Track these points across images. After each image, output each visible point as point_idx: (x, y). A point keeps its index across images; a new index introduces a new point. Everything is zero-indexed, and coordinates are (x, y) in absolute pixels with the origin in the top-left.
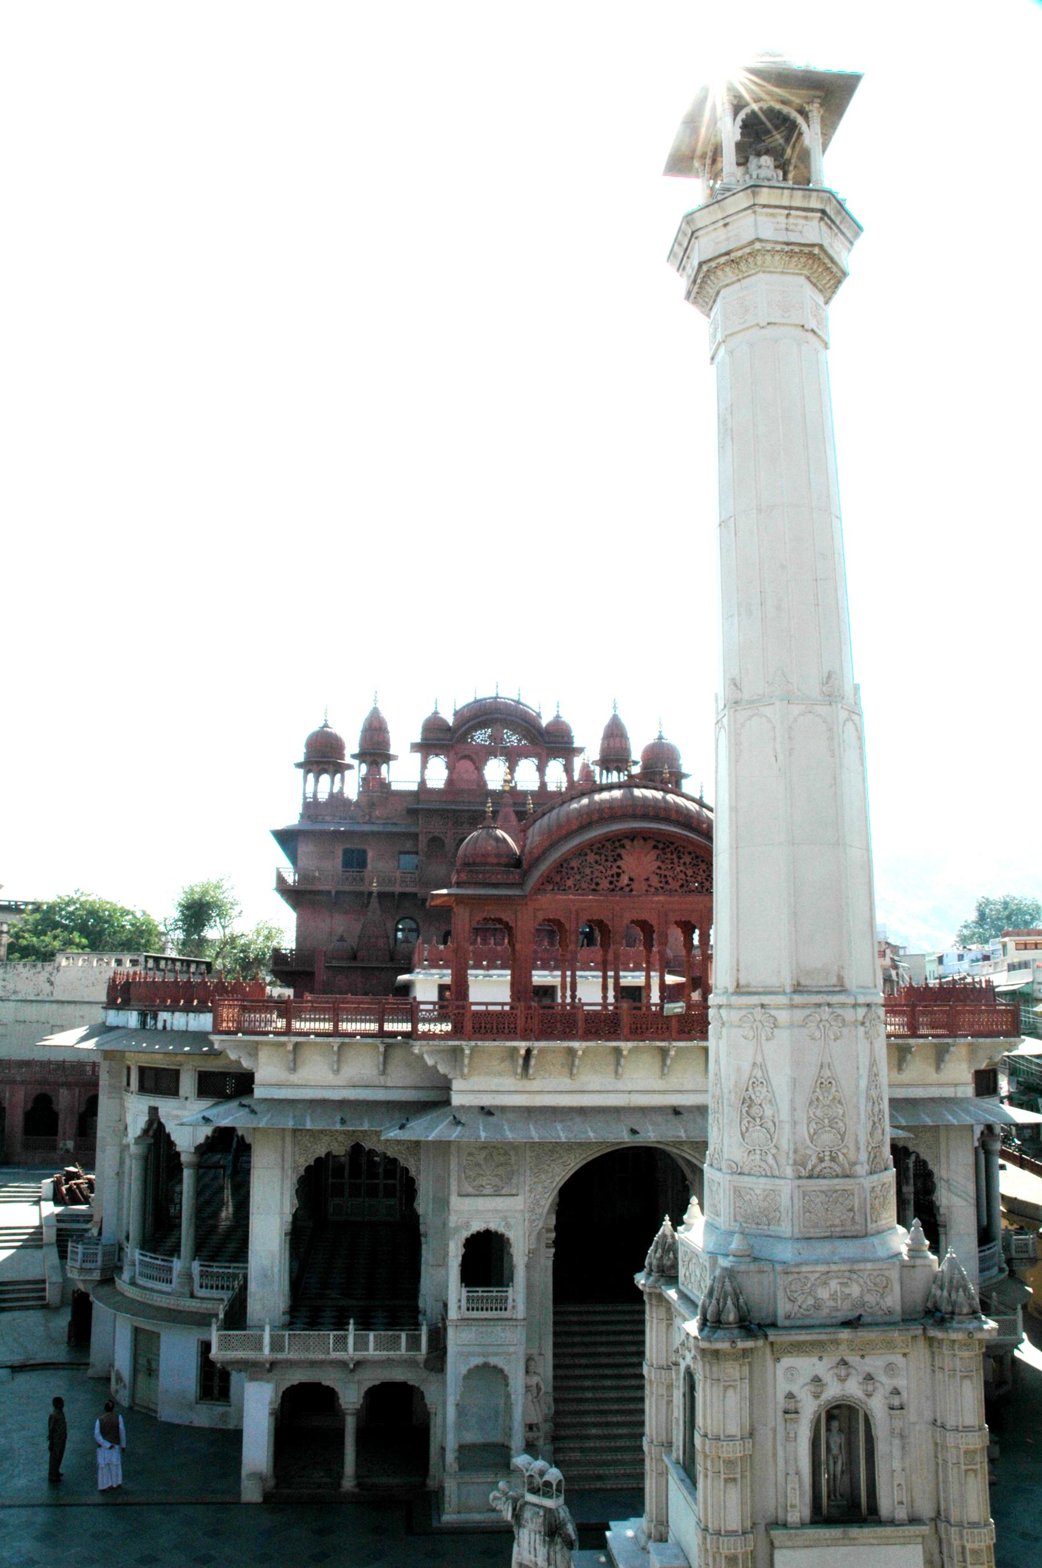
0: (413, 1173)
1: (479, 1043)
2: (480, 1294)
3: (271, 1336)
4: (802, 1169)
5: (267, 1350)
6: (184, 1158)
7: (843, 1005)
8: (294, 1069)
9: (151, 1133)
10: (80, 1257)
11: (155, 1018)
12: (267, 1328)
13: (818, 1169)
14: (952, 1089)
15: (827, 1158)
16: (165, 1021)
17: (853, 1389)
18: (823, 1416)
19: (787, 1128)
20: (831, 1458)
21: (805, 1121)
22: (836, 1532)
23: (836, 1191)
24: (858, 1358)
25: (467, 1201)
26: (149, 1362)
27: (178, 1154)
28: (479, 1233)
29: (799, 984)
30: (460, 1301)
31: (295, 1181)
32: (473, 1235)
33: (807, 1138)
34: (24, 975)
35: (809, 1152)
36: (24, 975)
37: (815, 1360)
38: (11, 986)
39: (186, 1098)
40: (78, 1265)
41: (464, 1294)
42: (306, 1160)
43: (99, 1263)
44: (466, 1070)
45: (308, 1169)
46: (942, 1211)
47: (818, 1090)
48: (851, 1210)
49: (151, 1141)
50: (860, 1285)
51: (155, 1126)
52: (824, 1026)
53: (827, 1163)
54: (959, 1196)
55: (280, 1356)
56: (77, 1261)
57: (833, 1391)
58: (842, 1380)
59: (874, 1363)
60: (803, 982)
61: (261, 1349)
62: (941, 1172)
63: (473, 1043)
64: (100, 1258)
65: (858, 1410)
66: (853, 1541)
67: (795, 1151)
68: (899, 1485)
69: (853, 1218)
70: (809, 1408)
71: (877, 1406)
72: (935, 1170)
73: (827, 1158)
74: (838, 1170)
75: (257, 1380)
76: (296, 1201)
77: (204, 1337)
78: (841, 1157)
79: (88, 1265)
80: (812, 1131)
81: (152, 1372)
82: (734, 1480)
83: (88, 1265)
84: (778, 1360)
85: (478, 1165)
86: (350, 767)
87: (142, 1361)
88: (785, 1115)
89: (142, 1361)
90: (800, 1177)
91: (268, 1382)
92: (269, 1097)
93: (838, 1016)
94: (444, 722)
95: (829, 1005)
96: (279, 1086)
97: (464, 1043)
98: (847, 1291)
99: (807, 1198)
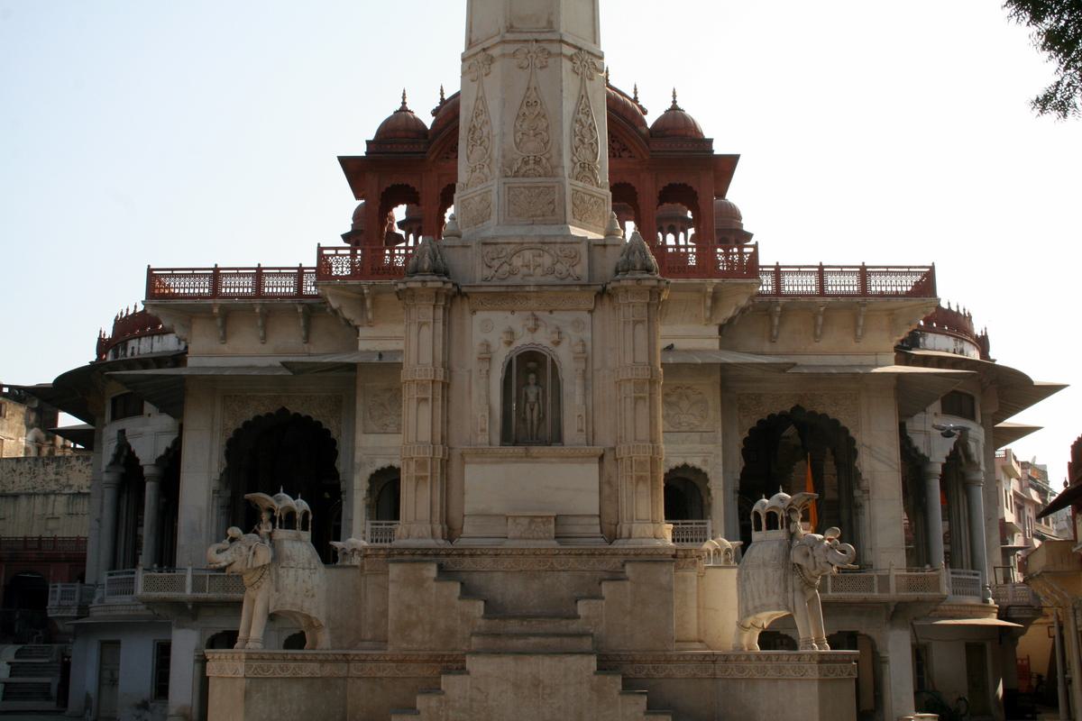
0: (334, 435)
1: (377, 282)
2: (384, 527)
3: (193, 576)
4: (508, 170)
5: (188, 591)
6: (147, 471)
7: (551, 41)
8: (224, 339)
9: (122, 460)
10: (58, 595)
11: (125, 349)
12: (190, 569)
13: (522, 171)
14: (874, 358)
15: (531, 162)
16: (133, 348)
17: (542, 339)
18: (514, 359)
19: (497, 140)
20: (528, 405)
21: (512, 132)
23: (539, 187)
24: (547, 313)
25: (372, 437)
26: (112, 674)
27: (141, 469)
28: (383, 469)
29: (512, 27)
30: (364, 532)
31: (224, 443)
32: (377, 471)
33: (514, 145)
34: (77, 468)
35: (515, 156)
36: (77, 468)
37: (508, 314)
38: (63, 480)
39: (149, 415)
40: (56, 603)
41: (369, 526)
42: (233, 425)
43: (77, 600)
44: (370, 315)
45: (237, 432)
46: (864, 476)
47: (525, 107)
48: (552, 202)
49: (123, 470)
50: (552, 255)
51: (125, 453)
52: (531, 56)
53: (531, 165)
54: (883, 462)
55: (202, 595)
56: (55, 599)
57: (524, 340)
58: (534, 330)
59: (560, 318)
60: (515, 24)
61: (184, 591)
62: (862, 438)
63: (371, 282)
64: (77, 596)
65: (546, 357)
66: (536, 459)
67: (504, 157)
68: (579, 416)
69: (554, 210)
70: (502, 355)
71: (565, 357)
72: (857, 437)
73: (531, 162)
74: (541, 171)
75: (184, 627)
76: (224, 462)
77: (162, 637)
78: (544, 161)
79: (65, 603)
80: (518, 140)
81: (114, 682)
82: (426, 400)
83: (65, 603)
84: (474, 312)
85: (382, 405)
86: (399, 239)
87: (107, 674)
88: (496, 131)
89: (107, 674)
90: (506, 177)
91: (194, 629)
92: (201, 365)
93: (544, 49)
95: (537, 41)
96: (210, 355)
97: (362, 282)
98: (539, 260)
99: (512, 193)
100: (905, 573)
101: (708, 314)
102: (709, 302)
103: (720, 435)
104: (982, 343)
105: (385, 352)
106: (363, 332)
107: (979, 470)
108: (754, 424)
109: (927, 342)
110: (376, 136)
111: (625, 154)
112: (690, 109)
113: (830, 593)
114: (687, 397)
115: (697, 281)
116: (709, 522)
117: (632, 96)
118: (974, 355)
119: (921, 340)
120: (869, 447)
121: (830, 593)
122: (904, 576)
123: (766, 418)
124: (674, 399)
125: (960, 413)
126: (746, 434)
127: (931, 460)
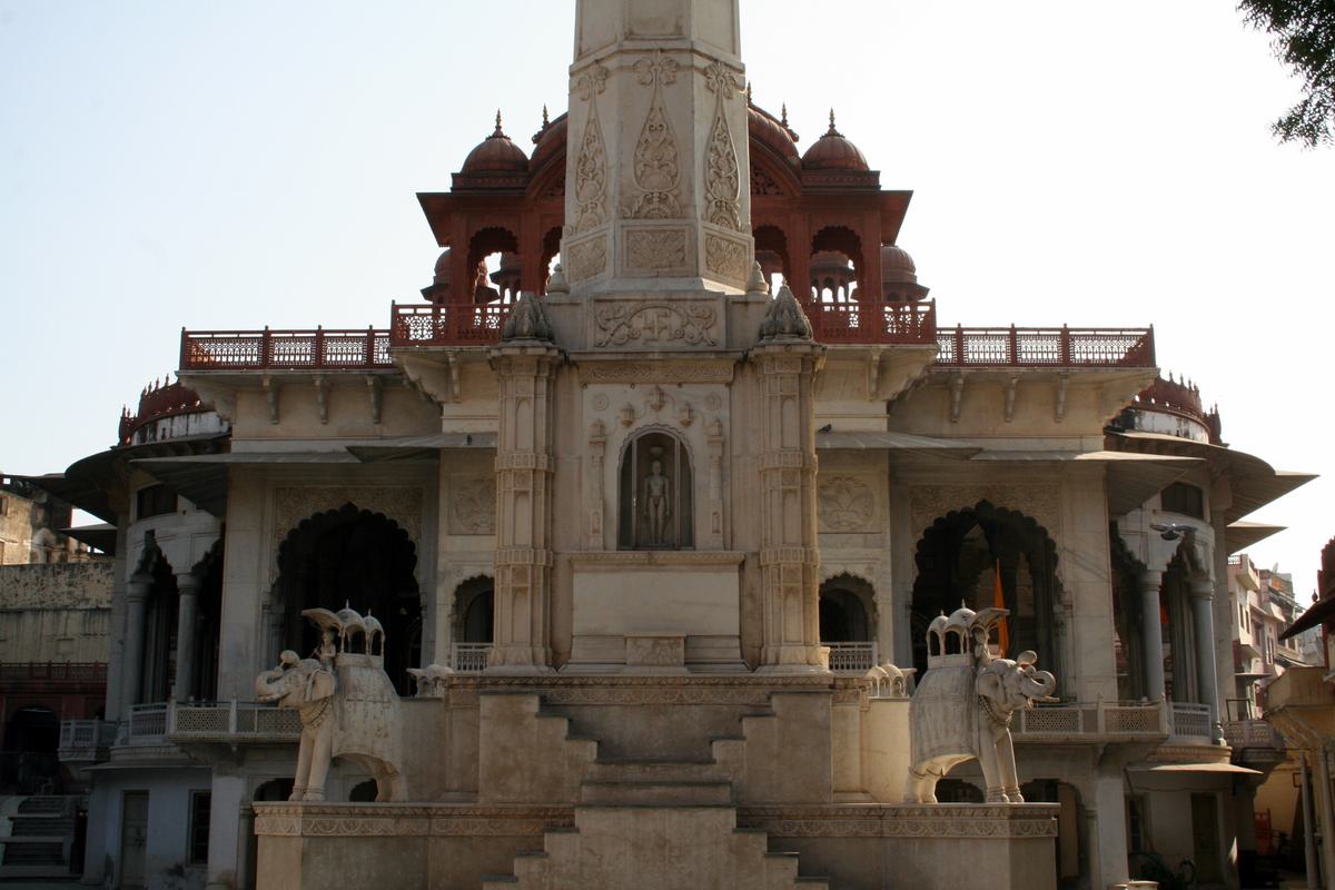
0: (412, 537)
1: (465, 348)
2: (473, 650)
3: (238, 711)
4: (626, 210)
5: (232, 730)
6: (182, 581)
7: (680, 51)
8: (277, 418)
9: (151, 568)
10: (72, 735)
11: (154, 431)
12: (234, 702)
13: (644, 211)
14: (1078, 441)
15: (656, 200)
16: (164, 429)
17: (669, 419)
18: (635, 443)
19: (613, 173)
20: (651, 500)
21: (632, 163)
22: (641, 555)
23: (665, 231)
24: (675, 387)
25: (458, 540)
26: (138, 832)
27: (174, 578)
28: (472, 579)
29: (631, 33)
30: (449, 657)
31: (277, 547)
32: (465, 582)
33: (634, 179)
34: (95, 577)
35: (635, 193)
36: (95, 577)
37: (627, 387)
38: (78, 592)
39: (184, 512)
40: (69, 744)
41: (455, 650)
42: (288, 525)
43: (95, 741)
44: (456, 389)
45: (293, 533)
46: (1066, 588)
47: (647, 133)
48: (681, 250)
49: (151, 580)
50: (681, 315)
51: (154, 559)
52: (656, 70)
53: (656, 204)
54: (1089, 570)
55: (249, 735)
56: (68, 739)
57: (646, 420)
58: (659, 407)
59: (692, 393)
60: (635, 30)
61: (227, 729)
62: (1064, 541)
63: (458, 348)
64: (95, 735)
65: (673, 440)
66: (661, 566)
67: (621, 193)
68: (715, 513)
69: (683, 259)
70: (619, 438)
71: (697, 441)
72: (1058, 540)
73: (656, 200)
74: (668, 211)
75: (227, 775)
76: (277, 570)
77: (199, 787)
78: (671, 198)
79: (80, 744)
80: (639, 173)
81: (141, 842)
82: (525, 493)
83: (80, 744)
84: (585, 385)
85: (472, 500)
86: (492, 294)
87: (131, 832)
88: (612, 161)
89: (131, 832)
90: (625, 218)
91: (239, 777)
92: (248, 451)
93: (671, 61)
94: (516, 151)
95: (662, 51)
96: (259, 438)
97: (447, 348)
98: (665, 321)
99: (631, 238)
100: (1117, 707)
101: (874, 388)
102: (875, 373)
103: (888, 537)
104: (1212, 423)
105: (474, 434)
106: (448, 410)
107: (1208, 580)
108: (930, 523)
109: (1143, 422)
110: (464, 168)
111: (771, 190)
112: (852, 134)
113: (1024, 732)
114: (848, 490)
115: (860, 346)
116: (875, 644)
117: (780, 119)
118: (1202, 438)
119: (1136, 420)
120: (1072, 552)
121: (1024, 732)
122: (1115, 711)
123: (945, 517)
124: (831, 492)
125: (1185, 510)
126: (921, 536)
127: (1149, 567)
